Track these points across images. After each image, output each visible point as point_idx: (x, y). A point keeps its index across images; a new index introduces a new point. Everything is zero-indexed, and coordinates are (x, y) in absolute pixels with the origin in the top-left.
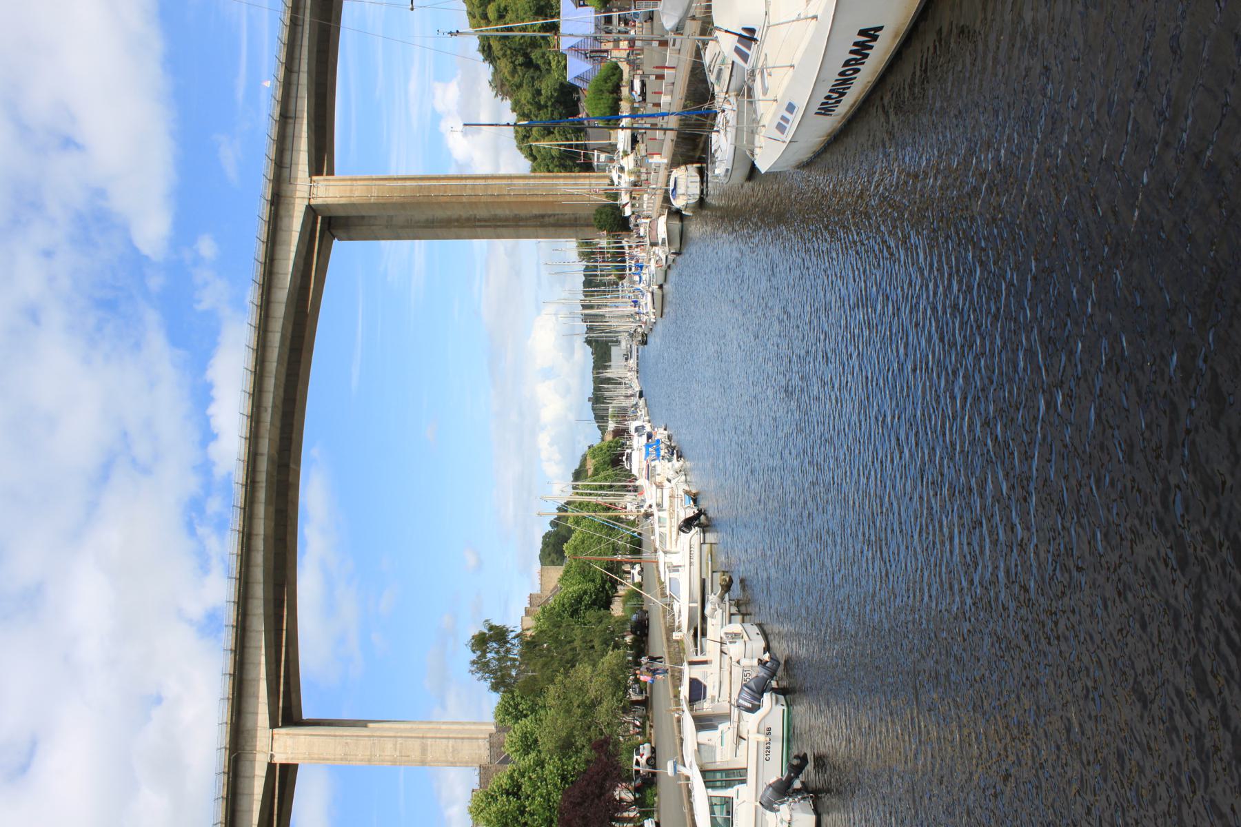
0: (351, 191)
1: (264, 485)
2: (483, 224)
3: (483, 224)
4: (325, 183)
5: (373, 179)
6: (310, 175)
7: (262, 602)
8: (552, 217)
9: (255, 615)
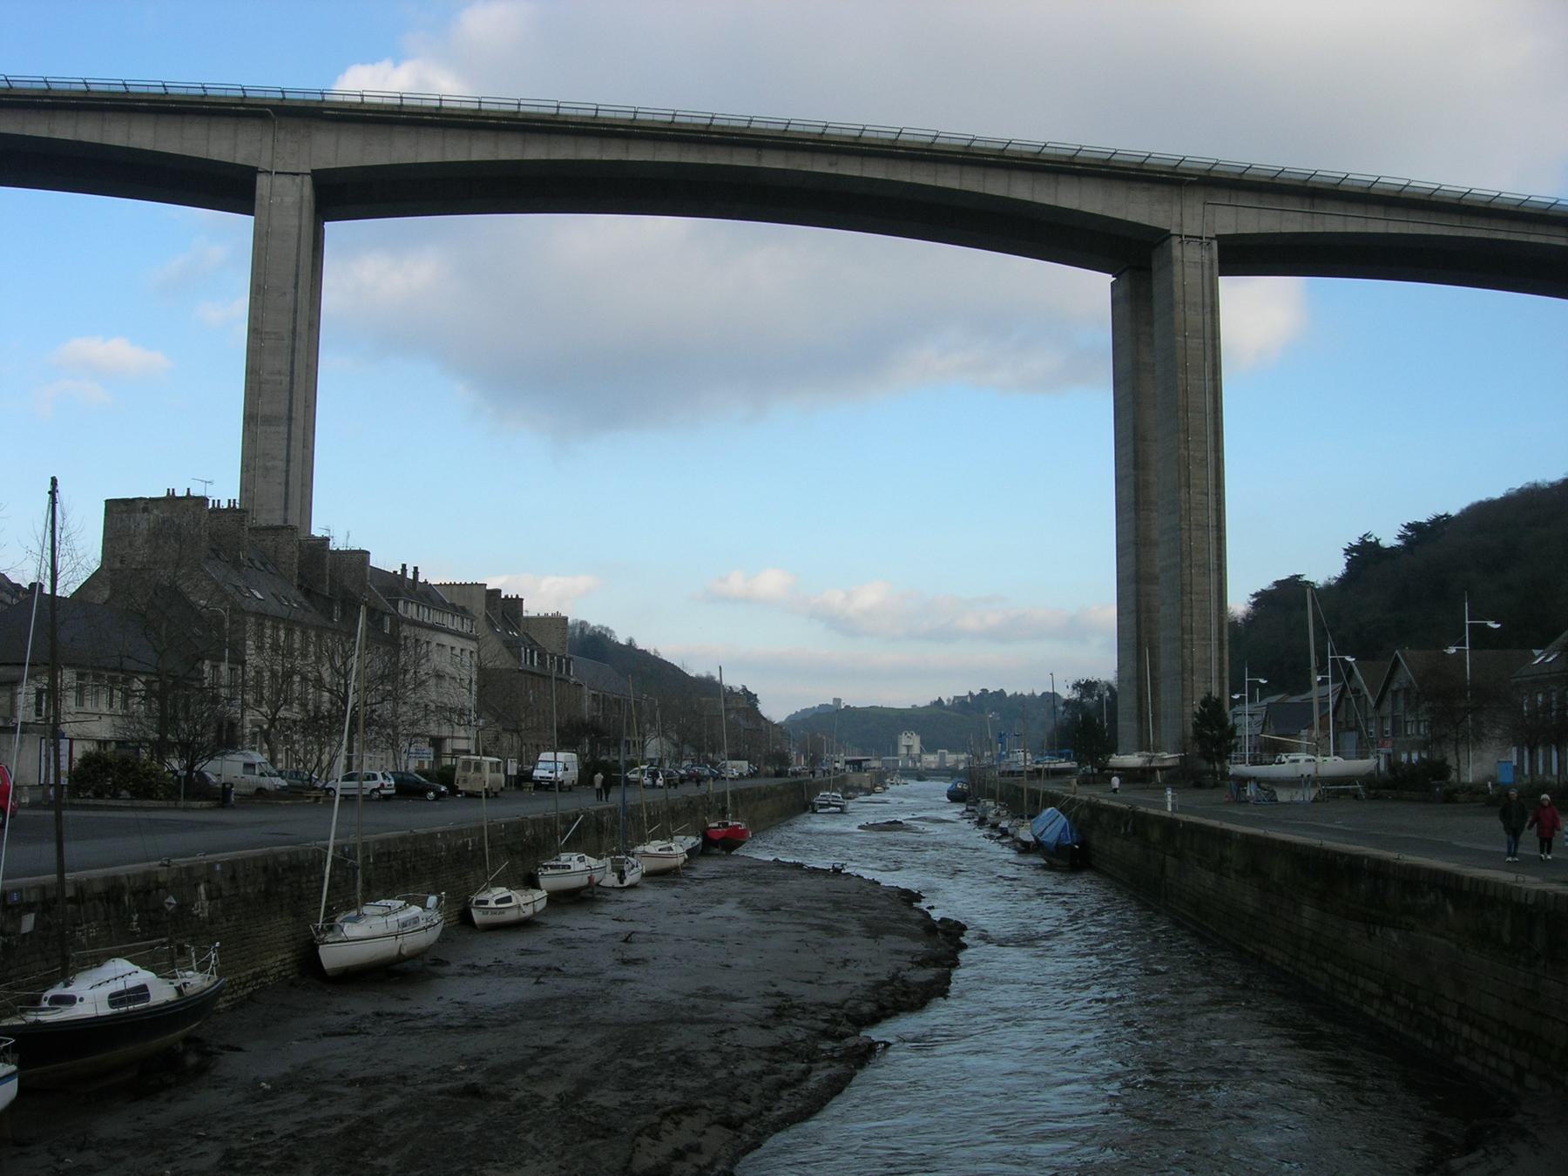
6: (1218, 237)
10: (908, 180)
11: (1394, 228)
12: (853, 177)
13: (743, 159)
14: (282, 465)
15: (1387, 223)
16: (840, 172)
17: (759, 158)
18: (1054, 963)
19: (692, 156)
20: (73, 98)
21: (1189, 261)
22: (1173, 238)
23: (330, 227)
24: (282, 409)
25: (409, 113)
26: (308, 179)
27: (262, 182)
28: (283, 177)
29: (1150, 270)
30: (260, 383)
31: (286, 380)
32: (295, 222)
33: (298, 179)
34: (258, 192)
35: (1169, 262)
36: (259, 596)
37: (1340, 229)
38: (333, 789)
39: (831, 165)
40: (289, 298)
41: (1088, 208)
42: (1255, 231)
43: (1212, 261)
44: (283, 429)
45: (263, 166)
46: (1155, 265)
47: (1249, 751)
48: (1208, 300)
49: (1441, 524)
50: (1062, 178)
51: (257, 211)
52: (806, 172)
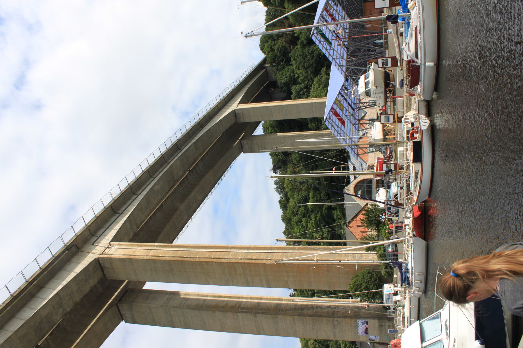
2: (245, 310)
3: (245, 310)
8: (311, 310)
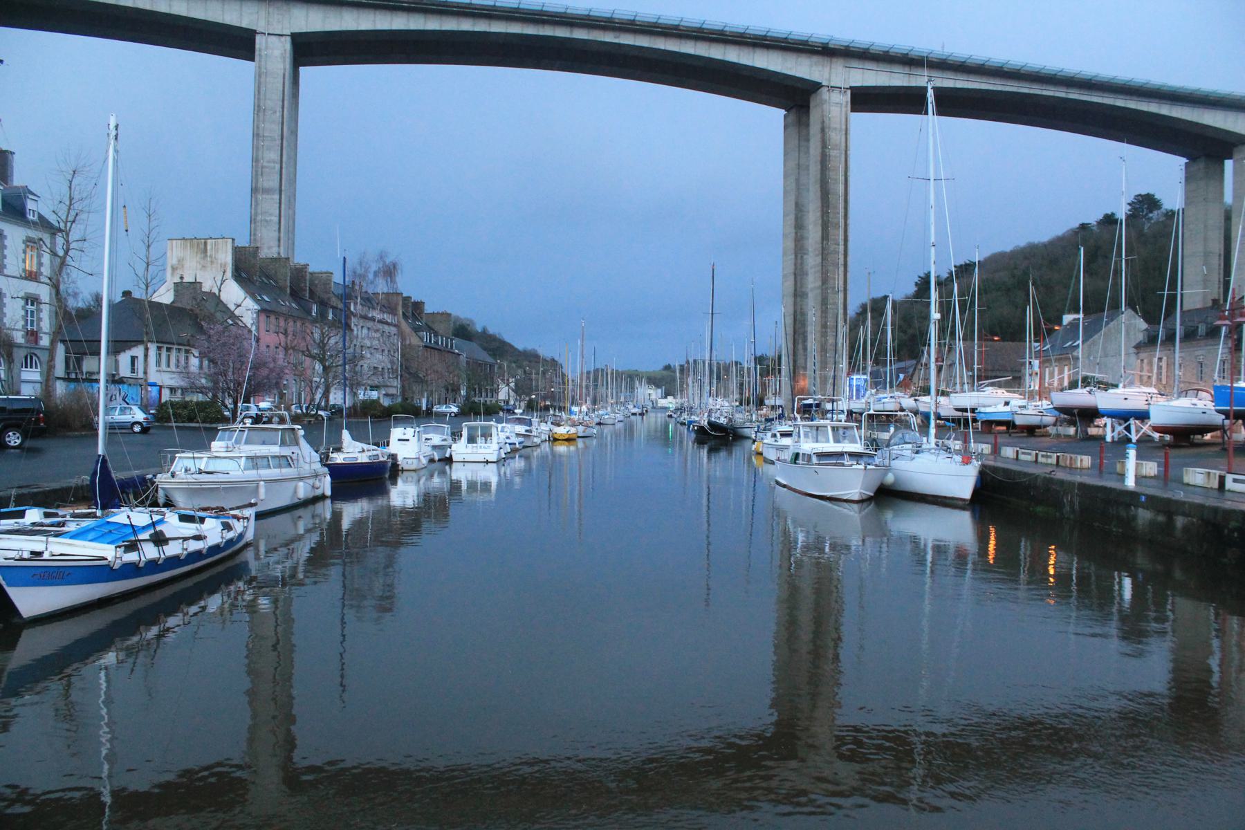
0: (835, 129)
1: (541, 33)
4: (844, 103)
5: (846, 152)
6: (851, 88)
7: (422, 28)
9: (408, 21)
10: (663, 48)
11: (959, 85)
12: (628, 45)
13: (561, 32)
14: (276, 219)
15: (863, 73)
16: (622, 42)
17: (473, 25)
18: (996, 591)
19: (530, 30)
20: (578, 19)
21: (834, 105)
22: (822, 89)
23: (302, 70)
24: (276, 184)
25: (640, 25)
26: (289, 39)
27: (259, 39)
28: (273, 37)
29: (808, 107)
30: (262, 167)
31: (278, 166)
32: (1217, 262)
33: (283, 39)
34: (257, 46)
35: (823, 102)
36: (267, 299)
37: (438, 28)
38: (841, 757)
39: (615, 37)
40: (279, 114)
41: (1184, 117)
42: (874, 84)
43: (847, 102)
44: (277, 197)
45: (259, 30)
46: (812, 104)
47: (886, 373)
48: (844, 127)
49: (1002, 255)
50: (430, 16)
51: (257, 58)
52: (601, 42)
